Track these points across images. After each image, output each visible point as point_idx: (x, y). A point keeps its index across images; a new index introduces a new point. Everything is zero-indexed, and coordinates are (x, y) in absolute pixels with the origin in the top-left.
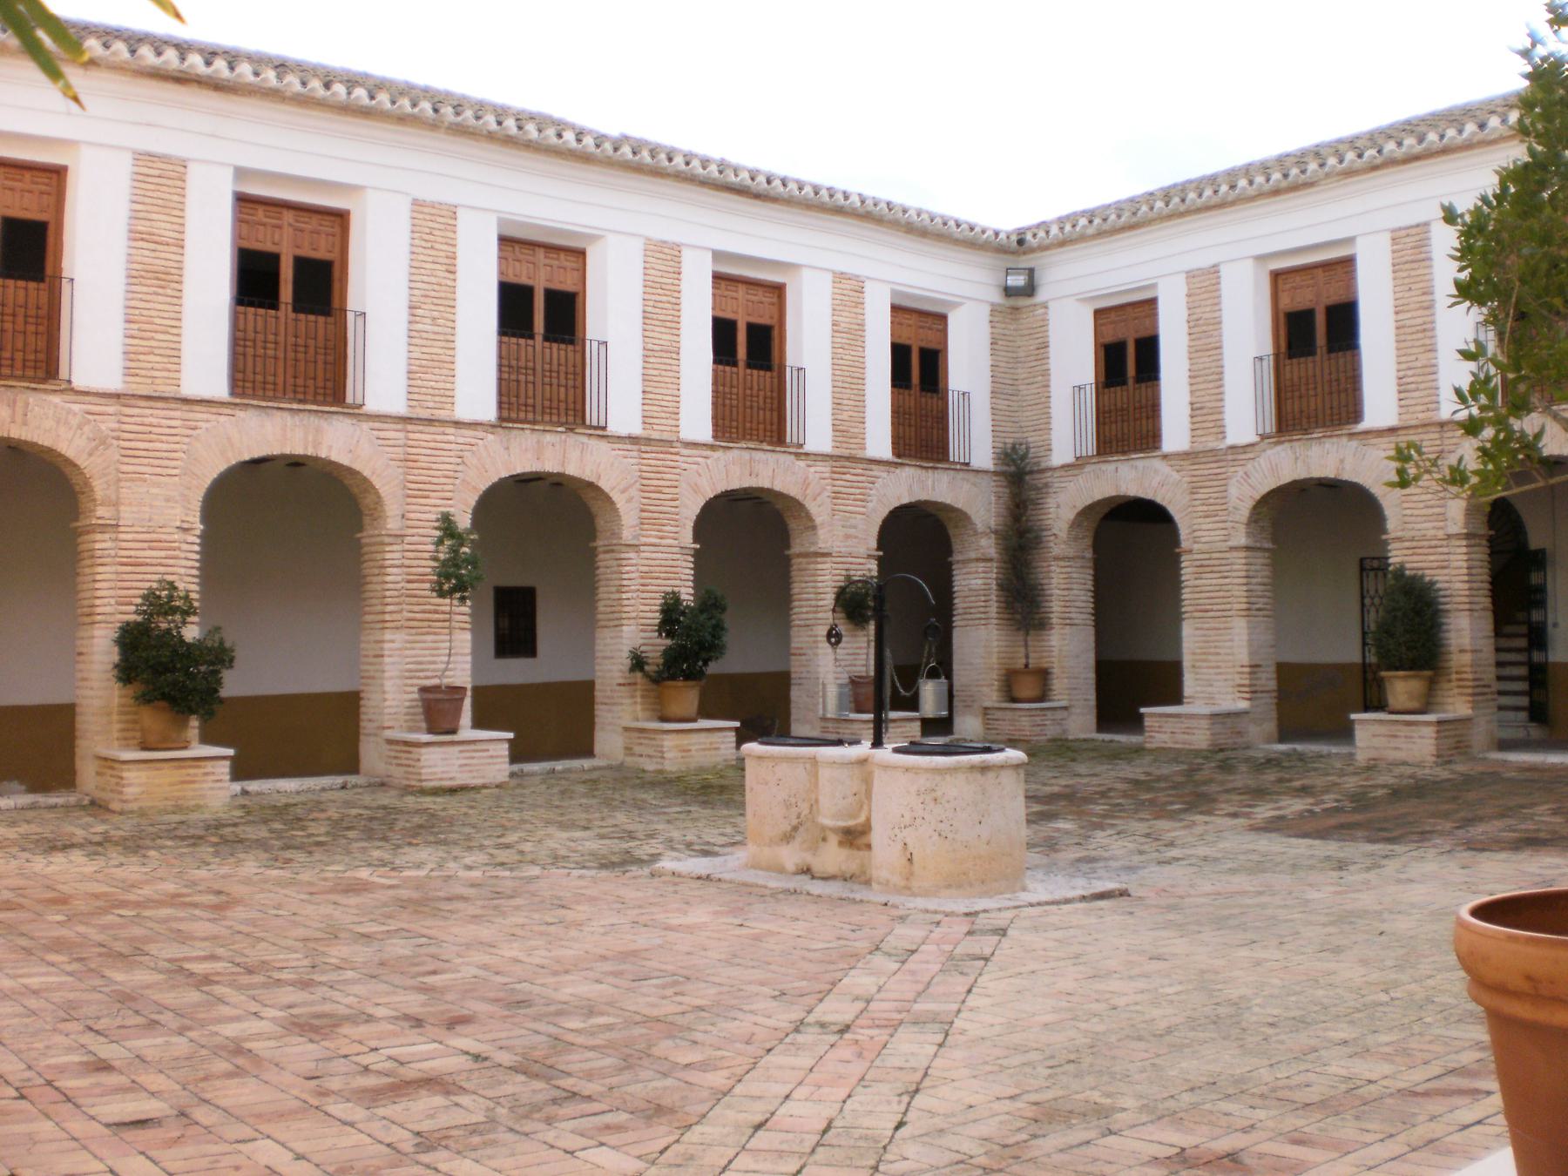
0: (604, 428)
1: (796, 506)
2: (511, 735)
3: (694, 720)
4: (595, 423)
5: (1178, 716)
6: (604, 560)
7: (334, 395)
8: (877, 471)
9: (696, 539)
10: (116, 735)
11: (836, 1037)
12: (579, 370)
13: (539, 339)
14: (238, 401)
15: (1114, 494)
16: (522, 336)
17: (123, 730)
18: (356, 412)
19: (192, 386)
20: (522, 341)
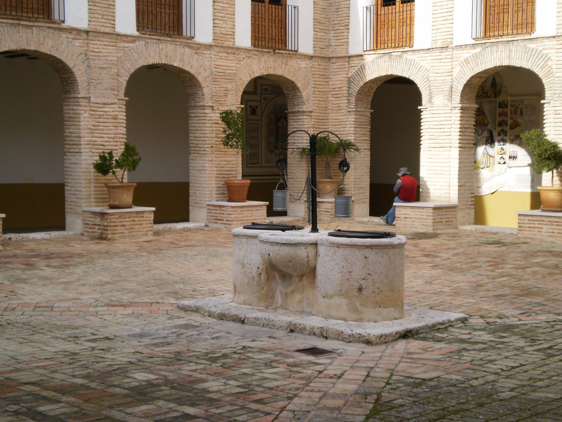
0: (297, 51)
1: (293, 87)
2: (154, 209)
3: (131, 207)
4: (290, 48)
5: (423, 208)
6: (194, 113)
7: (178, 32)
8: (243, 55)
9: (126, 95)
10: (93, 200)
11: (361, 358)
12: (283, 20)
13: (267, 3)
14: (256, 49)
15: (407, 77)
16: (277, 5)
17: (216, 191)
18: (59, 27)
19: (120, 29)
20: (260, 4)
